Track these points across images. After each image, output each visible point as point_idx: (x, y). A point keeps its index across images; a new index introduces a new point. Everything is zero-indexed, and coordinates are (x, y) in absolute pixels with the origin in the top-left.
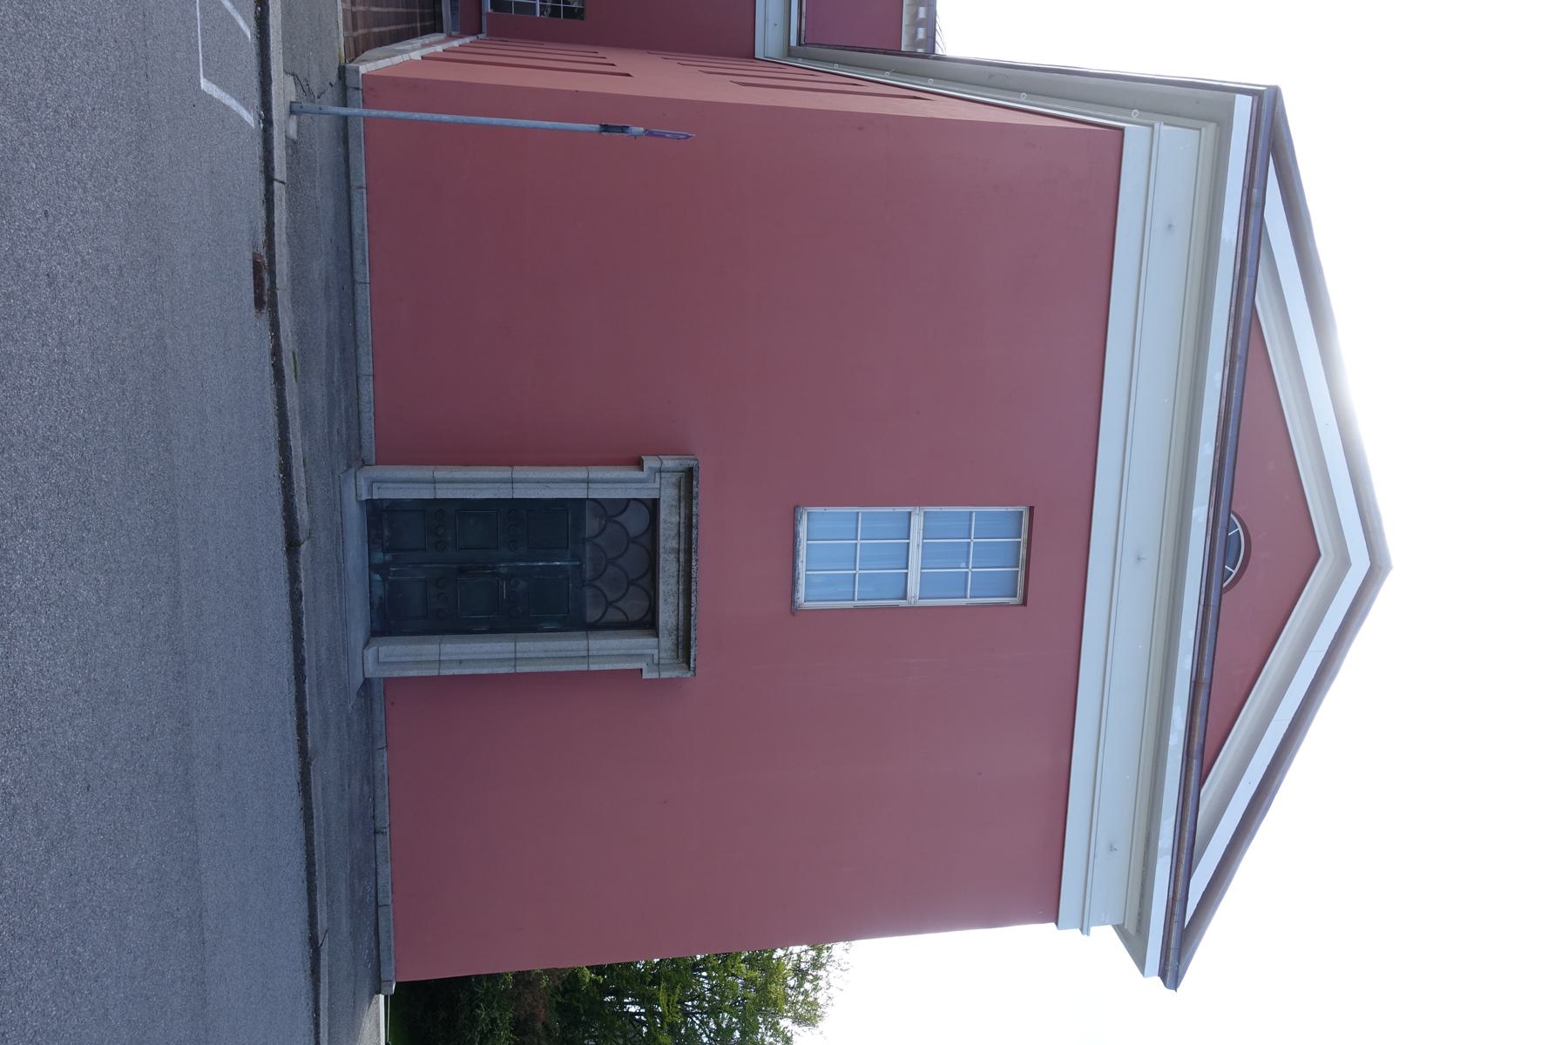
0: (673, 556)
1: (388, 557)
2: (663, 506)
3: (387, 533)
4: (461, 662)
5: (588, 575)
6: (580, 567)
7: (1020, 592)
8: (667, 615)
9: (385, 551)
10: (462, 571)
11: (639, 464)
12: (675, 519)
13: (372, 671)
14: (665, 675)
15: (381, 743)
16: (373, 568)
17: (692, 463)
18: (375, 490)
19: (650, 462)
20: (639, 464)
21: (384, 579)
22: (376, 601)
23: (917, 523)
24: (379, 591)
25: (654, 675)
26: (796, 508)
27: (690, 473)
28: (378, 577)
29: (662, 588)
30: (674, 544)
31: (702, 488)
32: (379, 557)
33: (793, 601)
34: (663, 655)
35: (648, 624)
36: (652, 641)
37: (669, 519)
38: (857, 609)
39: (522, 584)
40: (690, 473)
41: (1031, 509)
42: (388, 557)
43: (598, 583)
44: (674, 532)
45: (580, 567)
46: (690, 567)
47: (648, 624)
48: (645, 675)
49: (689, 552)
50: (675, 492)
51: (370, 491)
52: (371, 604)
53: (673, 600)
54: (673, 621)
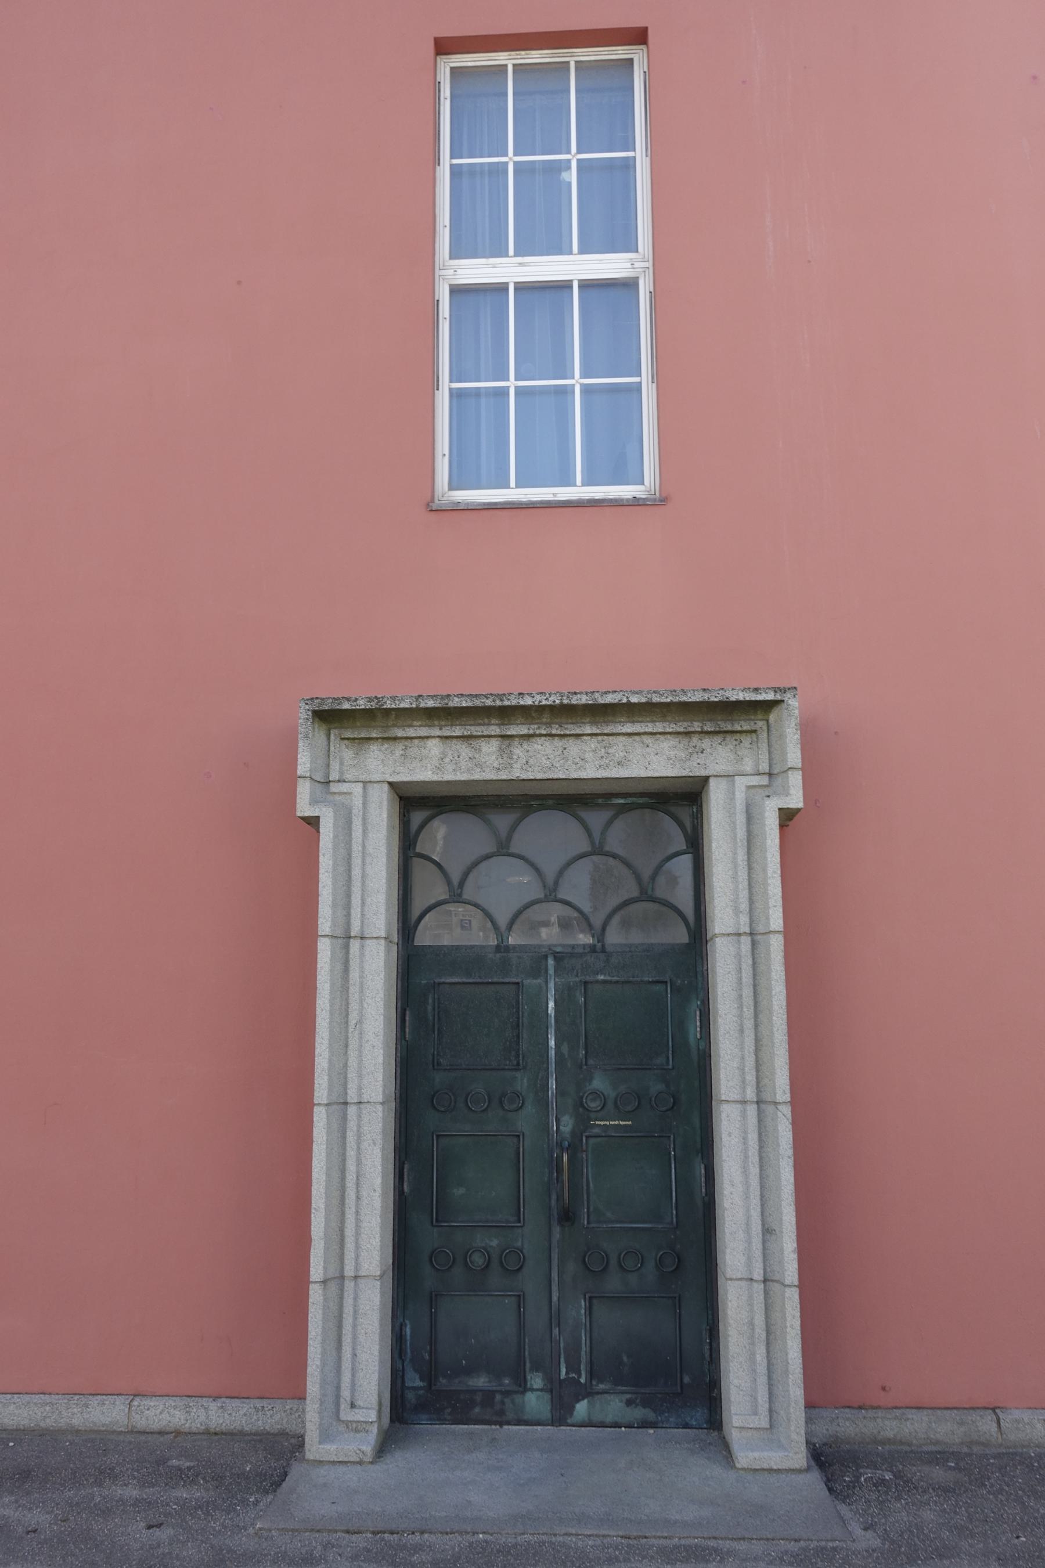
0: (519, 751)
1: (536, 1381)
2: (404, 776)
3: (481, 1382)
4: (767, 1231)
5: (584, 939)
6: (559, 958)
7: (619, 53)
8: (653, 758)
9: (522, 1386)
10: (567, 1217)
11: (313, 822)
12: (434, 747)
13: (794, 1454)
14: (794, 756)
15: (986, 1425)
16: (561, 1415)
17: (303, 713)
18: (358, 1415)
19: (304, 808)
20: (313, 822)
21: (587, 1393)
22: (639, 1413)
23: (475, 271)
24: (614, 1406)
25: (796, 779)
26: (433, 509)
27: (328, 717)
28: (581, 1408)
29: (590, 772)
30: (490, 749)
31: (358, 695)
32: (535, 1402)
33: (636, 502)
34: (748, 766)
35: (685, 799)
36: (716, 797)
37: (437, 761)
38: (658, 377)
39: (599, 1083)
40: (328, 717)
41: (444, 47)
42: (536, 1381)
43: (597, 921)
44: (464, 750)
45: (559, 958)
46: (541, 709)
47: (685, 799)
48: (795, 799)
49: (505, 713)
50: (374, 749)
51: (357, 1428)
52: (645, 1425)
53: (619, 747)
54: (668, 746)
